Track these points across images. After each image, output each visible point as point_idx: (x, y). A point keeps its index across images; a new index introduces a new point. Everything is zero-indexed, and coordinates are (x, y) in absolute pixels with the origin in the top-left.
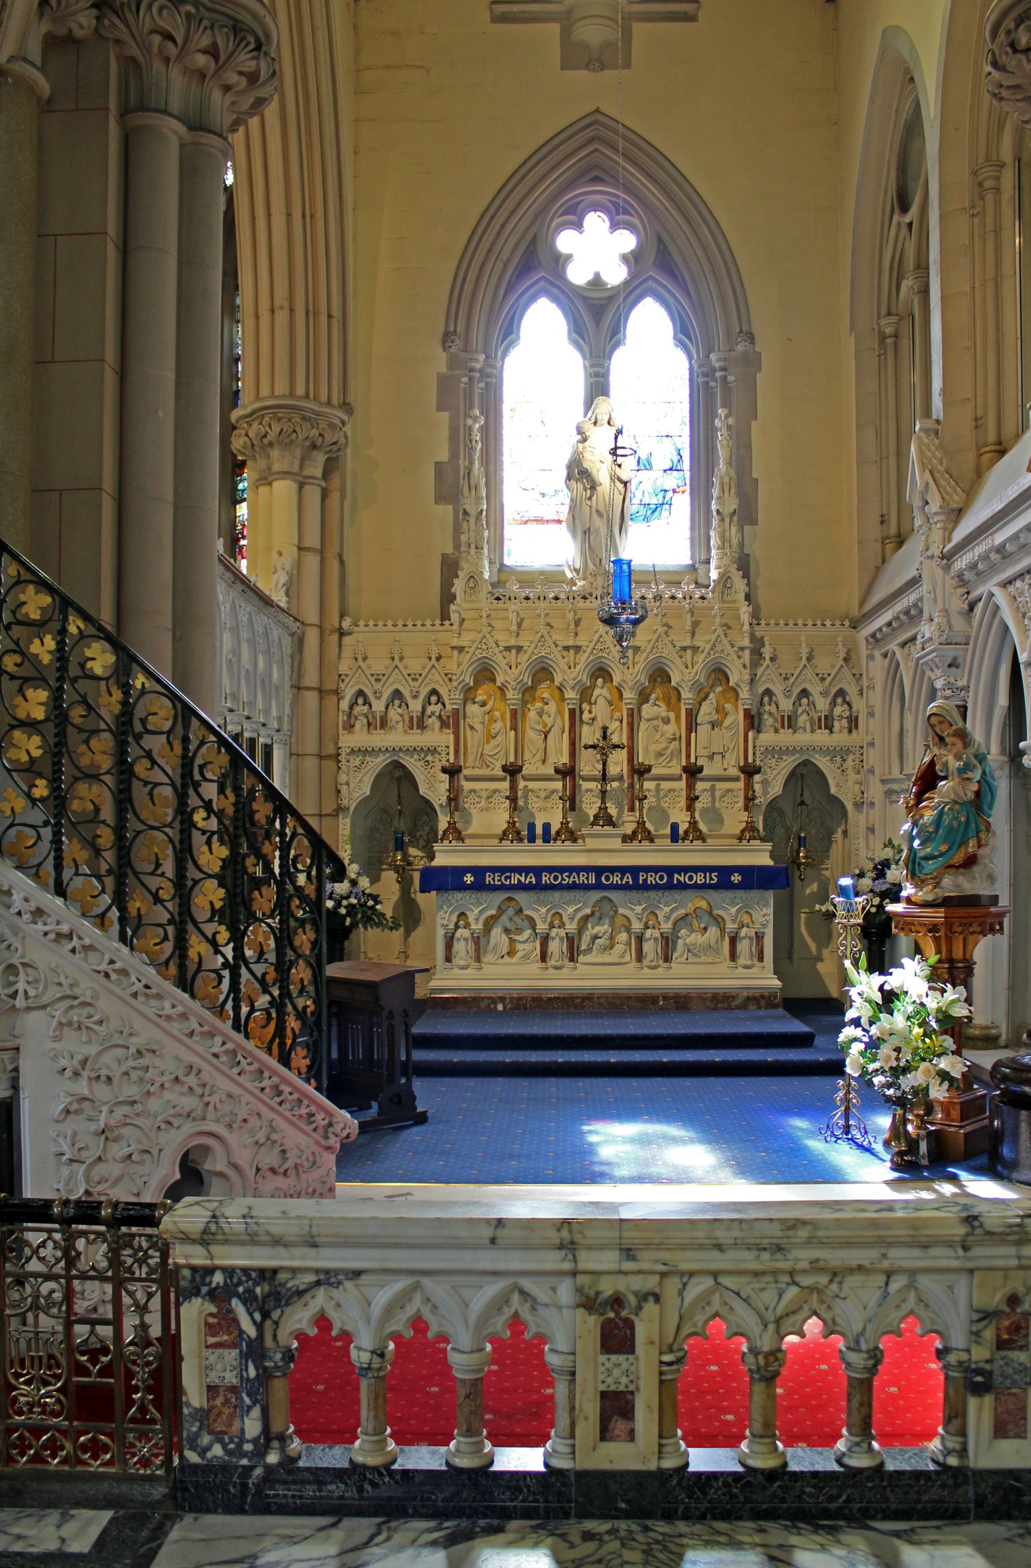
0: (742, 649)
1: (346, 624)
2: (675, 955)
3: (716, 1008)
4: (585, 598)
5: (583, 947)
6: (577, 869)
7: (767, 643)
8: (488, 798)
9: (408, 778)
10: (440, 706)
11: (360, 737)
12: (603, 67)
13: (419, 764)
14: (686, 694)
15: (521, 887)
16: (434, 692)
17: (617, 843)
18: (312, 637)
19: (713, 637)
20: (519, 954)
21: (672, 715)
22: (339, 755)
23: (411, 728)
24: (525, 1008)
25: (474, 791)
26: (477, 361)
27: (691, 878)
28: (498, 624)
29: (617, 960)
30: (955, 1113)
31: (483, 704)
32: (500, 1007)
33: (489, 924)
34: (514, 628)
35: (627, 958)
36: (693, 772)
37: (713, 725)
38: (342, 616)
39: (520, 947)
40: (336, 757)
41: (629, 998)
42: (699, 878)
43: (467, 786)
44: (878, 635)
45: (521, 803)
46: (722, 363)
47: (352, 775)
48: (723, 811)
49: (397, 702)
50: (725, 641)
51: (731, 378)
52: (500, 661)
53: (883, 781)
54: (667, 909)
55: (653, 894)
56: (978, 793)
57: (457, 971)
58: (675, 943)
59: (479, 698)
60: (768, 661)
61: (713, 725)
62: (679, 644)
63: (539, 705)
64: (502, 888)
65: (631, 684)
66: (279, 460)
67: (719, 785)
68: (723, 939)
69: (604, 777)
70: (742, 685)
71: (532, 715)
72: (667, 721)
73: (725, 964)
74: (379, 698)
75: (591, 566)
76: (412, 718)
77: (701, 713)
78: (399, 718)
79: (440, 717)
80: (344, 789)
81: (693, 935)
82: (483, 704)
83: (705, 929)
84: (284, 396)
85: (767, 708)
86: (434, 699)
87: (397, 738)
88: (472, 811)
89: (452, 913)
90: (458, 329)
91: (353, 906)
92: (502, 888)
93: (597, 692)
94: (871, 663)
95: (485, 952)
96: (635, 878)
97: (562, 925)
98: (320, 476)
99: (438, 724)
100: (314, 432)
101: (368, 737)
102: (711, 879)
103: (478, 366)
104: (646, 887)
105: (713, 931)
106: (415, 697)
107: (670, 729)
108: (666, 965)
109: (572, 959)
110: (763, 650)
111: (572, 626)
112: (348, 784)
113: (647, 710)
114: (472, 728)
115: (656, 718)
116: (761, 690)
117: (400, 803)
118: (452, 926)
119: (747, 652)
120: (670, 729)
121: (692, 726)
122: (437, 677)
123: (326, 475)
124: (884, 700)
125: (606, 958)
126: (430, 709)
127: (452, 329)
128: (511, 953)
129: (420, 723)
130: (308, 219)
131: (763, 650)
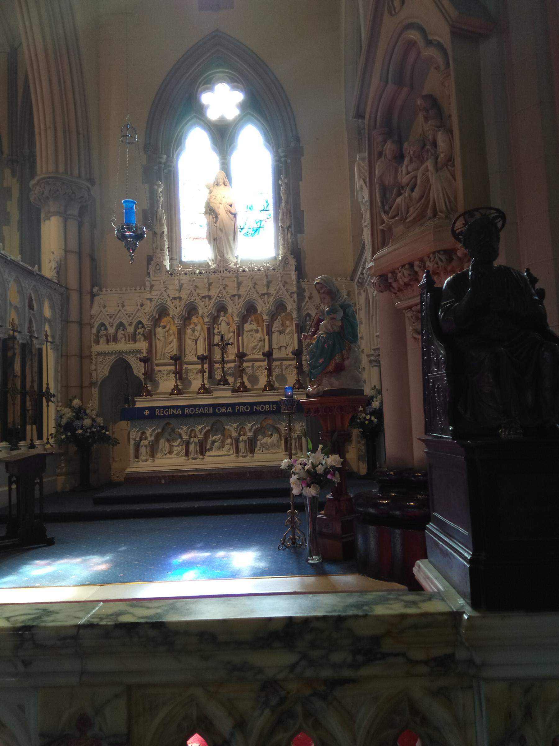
0: (292, 293)
1: (96, 290)
2: (256, 450)
4: (215, 272)
5: (208, 447)
7: (307, 290)
9: (128, 367)
10: (143, 329)
11: (103, 347)
13: (133, 359)
15: (174, 416)
16: (140, 322)
18: (74, 297)
19: (277, 288)
20: (175, 452)
21: (260, 329)
22: (91, 356)
23: (129, 341)
25: (160, 371)
28: (171, 287)
29: (226, 453)
30: (299, 500)
31: (164, 327)
32: (163, 481)
35: (231, 452)
36: (268, 355)
37: (281, 332)
38: (93, 286)
40: (90, 357)
42: (267, 408)
44: (360, 281)
45: (184, 376)
48: (287, 376)
49: (121, 328)
52: (171, 305)
54: (250, 425)
56: (342, 327)
58: (256, 443)
61: (281, 332)
63: (192, 326)
64: (164, 417)
66: (53, 206)
68: (281, 440)
71: (189, 331)
72: (257, 331)
73: (283, 453)
74: (112, 326)
75: (219, 257)
77: (274, 327)
78: (122, 336)
79: (143, 335)
80: (94, 373)
81: (265, 439)
82: (164, 327)
86: (140, 326)
87: (122, 346)
88: (160, 381)
89: (138, 431)
91: (93, 432)
93: (221, 318)
95: (157, 452)
99: (142, 339)
101: (107, 346)
102: (273, 408)
106: (130, 325)
107: (258, 335)
112: (96, 370)
113: (247, 327)
114: (159, 339)
115: (252, 330)
118: (138, 439)
120: (258, 335)
125: (221, 453)
126: (138, 331)
128: (170, 453)
131: (305, 294)
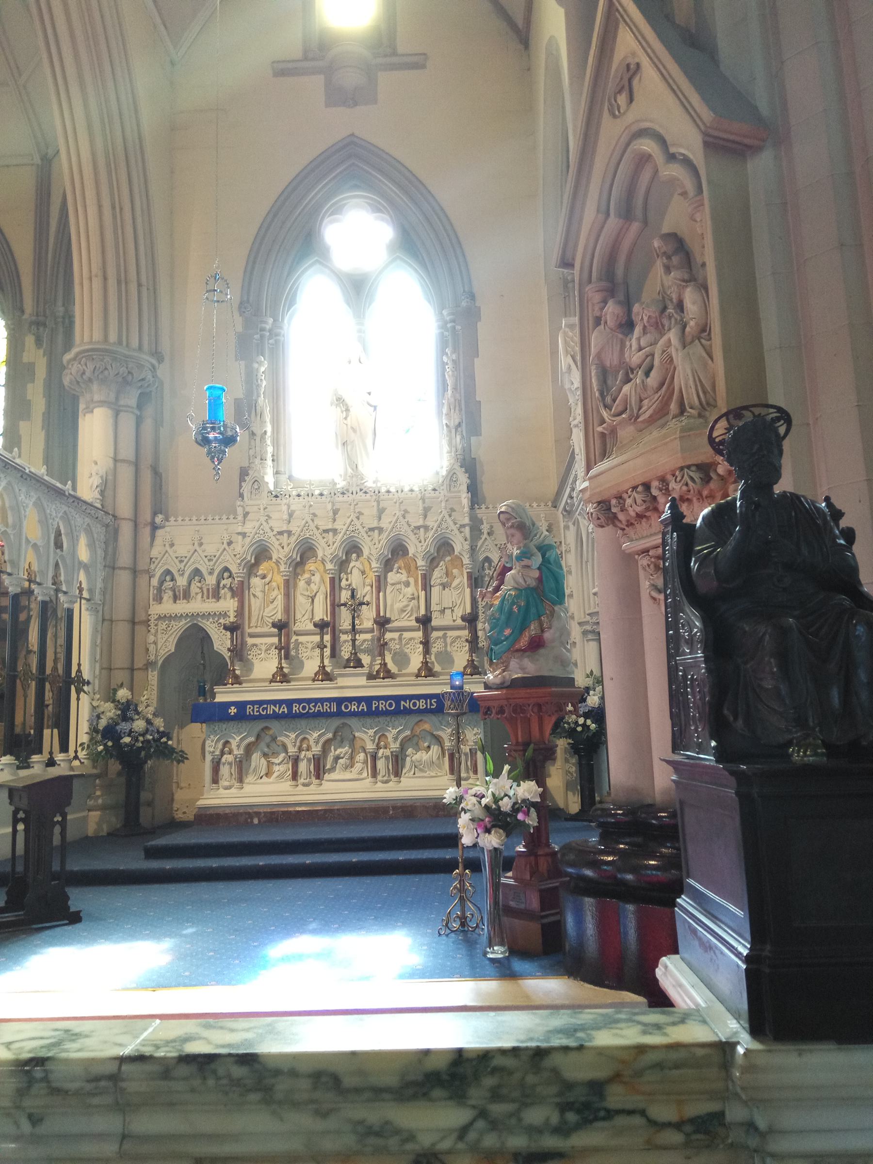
0: (463, 526)
1: (159, 519)
3: (437, 816)
4: (343, 493)
5: (328, 767)
6: (322, 701)
8: (266, 650)
9: (206, 639)
10: (230, 580)
11: (168, 607)
12: (356, 104)
14: (420, 563)
15: (276, 716)
16: (226, 569)
17: (363, 681)
18: (126, 530)
21: (411, 580)
23: (208, 598)
24: (277, 821)
25: (256, 645)
26: (265, 322)
27: (415, 704)
28: (274, 516)
32: (256, 821)
33: (249, 750)
34: (286, 517)
35: (365, 774)
38: (155, 514)
39: (276, 768)
40: (146, 622)
41: (363, 809)
42: (421, 704)
43: (250, 641)
45: (293, 653)
46: (452, 317)
47: (159, 636)
50: (449, 520)
51: (458, 327)
53: (580, 624)
55: (382, 719)
57: (221, 791)
58: (404, 760)
59: (260, 572)
60: (485, 536)
61: (444, 586)
62: (414, 524)
63: (306, 576)
64: (260, 717)
65: (376, 556)
66: (98, 393)
67: (450, 633)
69: (354, 630)
70: (464, 554)
71: (301, 584)
72: (407, 584)
73: (446, 777)
74: (182, 575)
75: (350, 470)
76: (208, 590)
77: (434, 577)
78: (198, 590)
79: (231, 589)
80: (152, 648)
81: (419, 753)
83: (429, 747)
84: (99, 342)
85: (487, 572)
86: (226, 575)
87: (197, 605)
90: (251, 299)
91: (148, 741)
92: (260, 717)
94: (567, 532)
96: (369, 706)
97: (308, 749)
98: (135, 406)
99: (229, 595)
100: (123, 370)
102: (431, 704)
103: (268, 327)
104: (378, 713)
105: (435, 749)
106: (211, 573)
107: (410, 590)
108: (396, 779)
109: (318, 777)
110: (482, 526)
111: (331, 514)
112: (155, 643)
113: (392, 577)
114: (254, 596)
115: (399, 583)
116: (481, 558)
117: (203, 658)
118: (218, 753)
119: (467, 529)
120: (410, 590)
121: (427, 586)
122: (228, 557)
123: (140, 406)
124: (576, 559)
125: (348, 775)
127: (245, 299)
128: (268, 774)
129: (216, 594)
130: (118, 210)
